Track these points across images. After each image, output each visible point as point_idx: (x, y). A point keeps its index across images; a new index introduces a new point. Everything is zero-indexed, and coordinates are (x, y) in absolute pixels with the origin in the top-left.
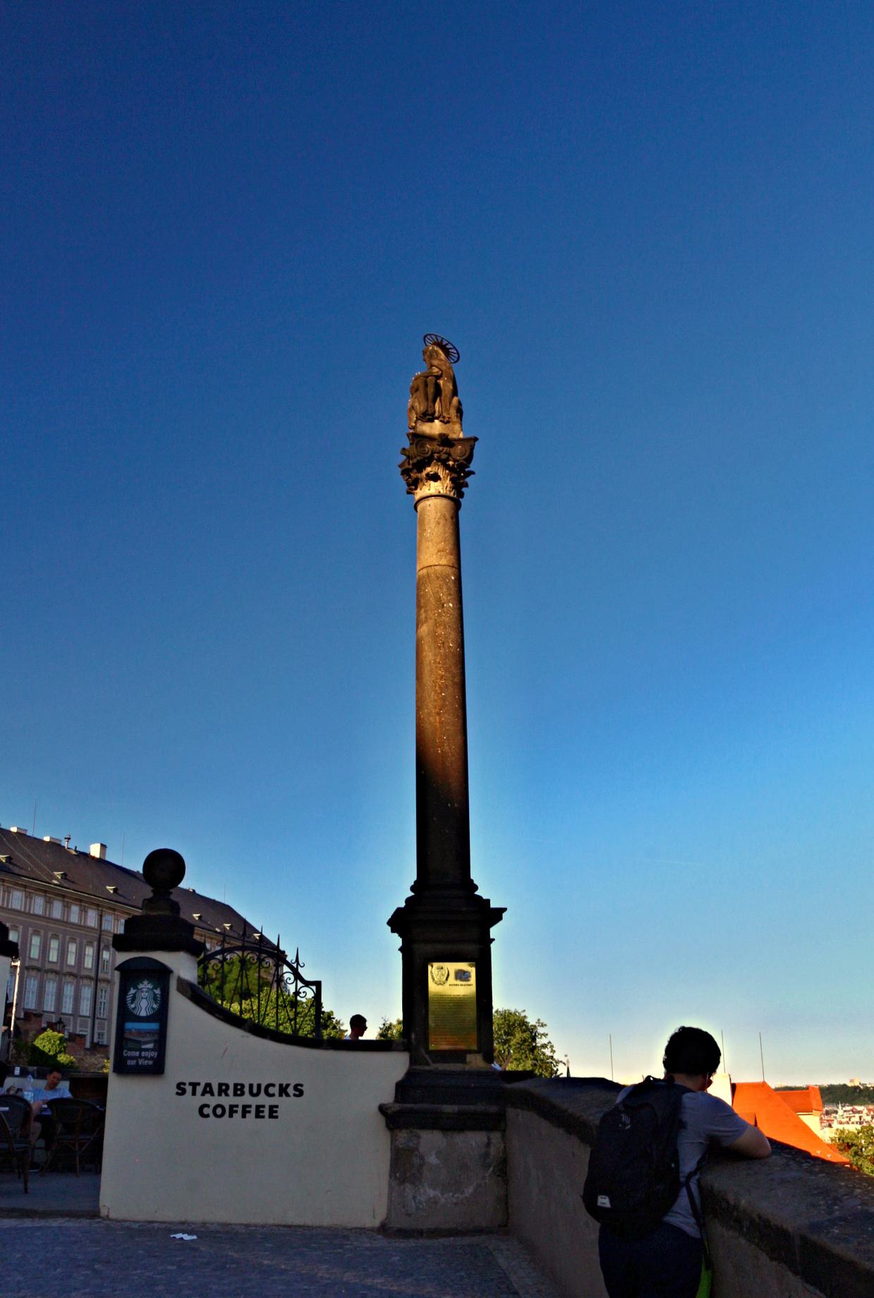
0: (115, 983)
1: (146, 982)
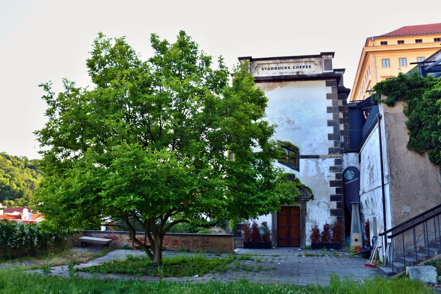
0: (200, 260)
1: (348, 171)
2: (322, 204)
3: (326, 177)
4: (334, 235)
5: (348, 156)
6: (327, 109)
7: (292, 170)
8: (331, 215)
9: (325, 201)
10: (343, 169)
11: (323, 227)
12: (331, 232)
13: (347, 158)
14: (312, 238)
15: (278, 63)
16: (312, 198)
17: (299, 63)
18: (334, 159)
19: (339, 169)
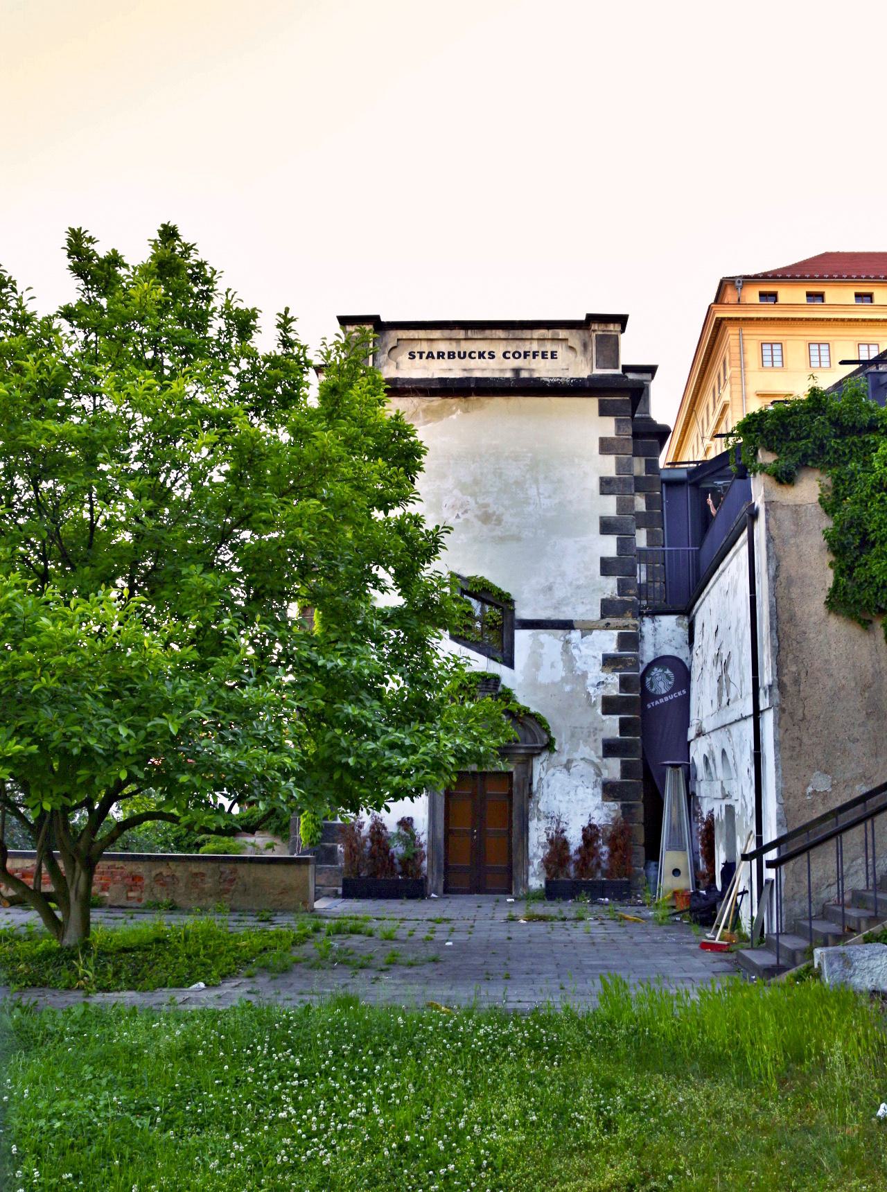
1: (656, 669)
2: (580, 767)
3: (593, 685)
4: (611, 856)
5: (657, 624)
6: (601, 485)
7: (493, 663)
8: (604, 799)
9: (587, 757)
10: (642, 662)
11: (580, 835)
12: (605, 849)
13: (655, 630)
14: (547, 867)
15: (458, 340)
16: (549, 746)
17: (520, 343)
18: (616, 633)
19: (630, 661)
